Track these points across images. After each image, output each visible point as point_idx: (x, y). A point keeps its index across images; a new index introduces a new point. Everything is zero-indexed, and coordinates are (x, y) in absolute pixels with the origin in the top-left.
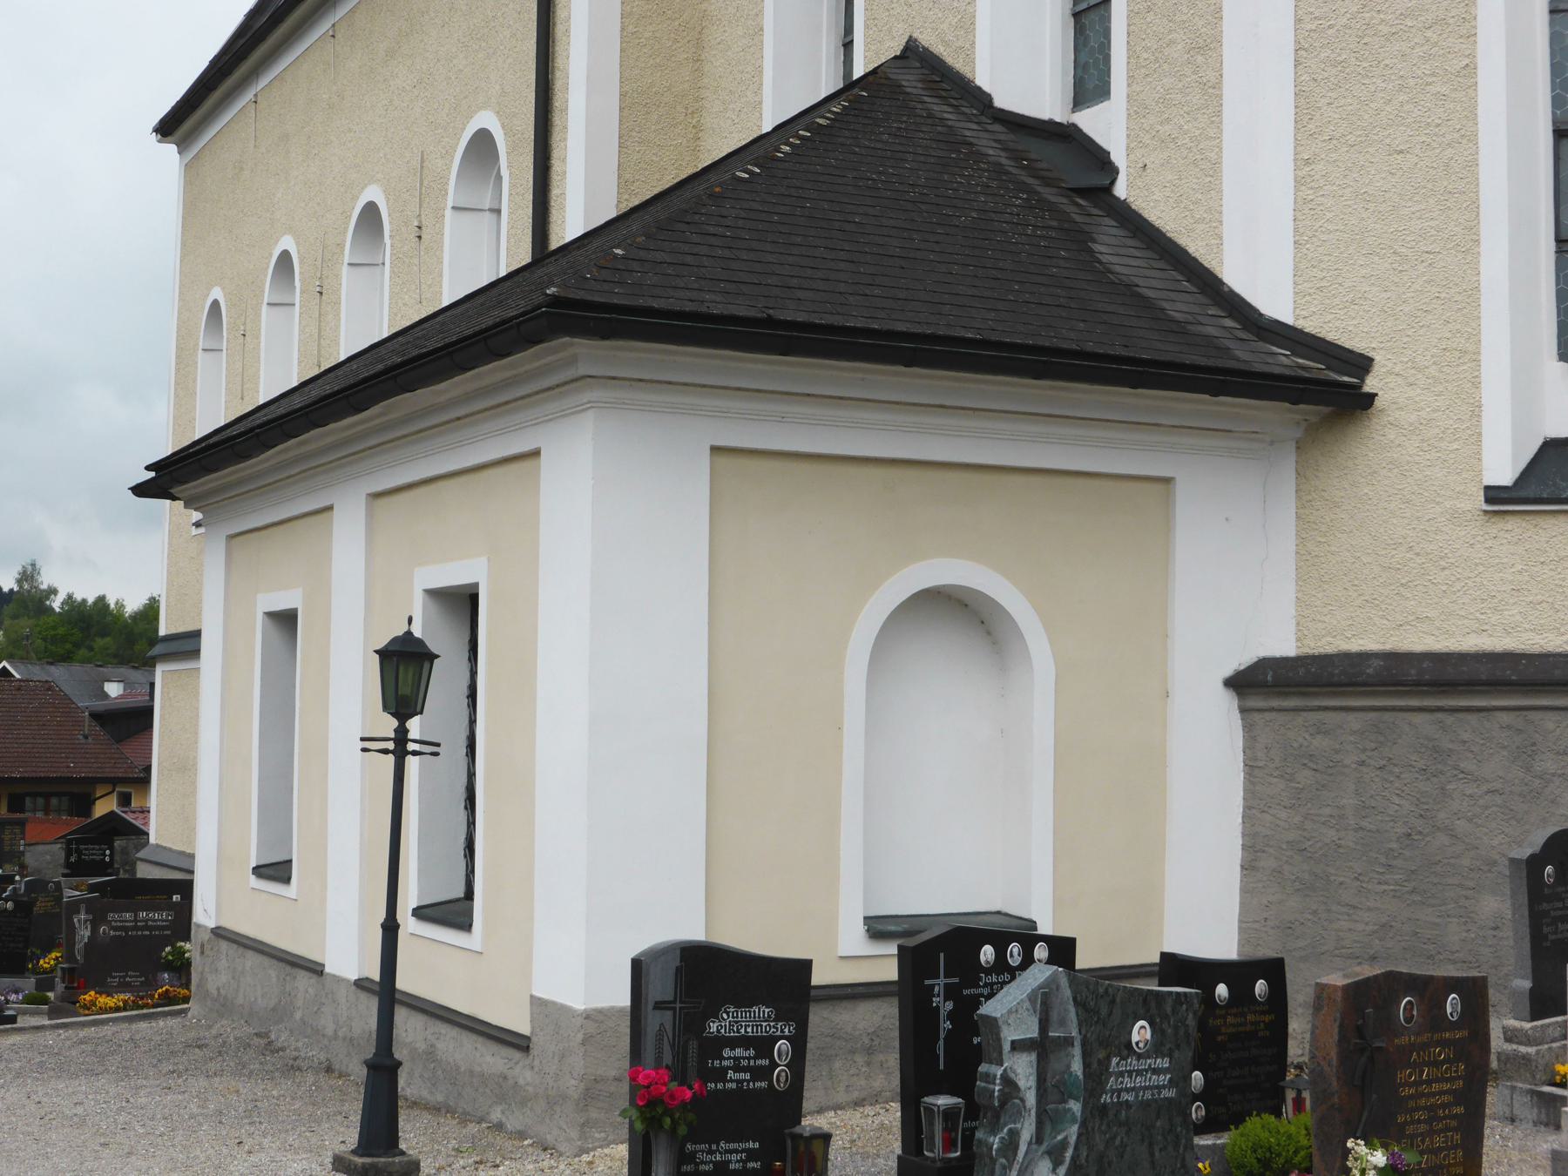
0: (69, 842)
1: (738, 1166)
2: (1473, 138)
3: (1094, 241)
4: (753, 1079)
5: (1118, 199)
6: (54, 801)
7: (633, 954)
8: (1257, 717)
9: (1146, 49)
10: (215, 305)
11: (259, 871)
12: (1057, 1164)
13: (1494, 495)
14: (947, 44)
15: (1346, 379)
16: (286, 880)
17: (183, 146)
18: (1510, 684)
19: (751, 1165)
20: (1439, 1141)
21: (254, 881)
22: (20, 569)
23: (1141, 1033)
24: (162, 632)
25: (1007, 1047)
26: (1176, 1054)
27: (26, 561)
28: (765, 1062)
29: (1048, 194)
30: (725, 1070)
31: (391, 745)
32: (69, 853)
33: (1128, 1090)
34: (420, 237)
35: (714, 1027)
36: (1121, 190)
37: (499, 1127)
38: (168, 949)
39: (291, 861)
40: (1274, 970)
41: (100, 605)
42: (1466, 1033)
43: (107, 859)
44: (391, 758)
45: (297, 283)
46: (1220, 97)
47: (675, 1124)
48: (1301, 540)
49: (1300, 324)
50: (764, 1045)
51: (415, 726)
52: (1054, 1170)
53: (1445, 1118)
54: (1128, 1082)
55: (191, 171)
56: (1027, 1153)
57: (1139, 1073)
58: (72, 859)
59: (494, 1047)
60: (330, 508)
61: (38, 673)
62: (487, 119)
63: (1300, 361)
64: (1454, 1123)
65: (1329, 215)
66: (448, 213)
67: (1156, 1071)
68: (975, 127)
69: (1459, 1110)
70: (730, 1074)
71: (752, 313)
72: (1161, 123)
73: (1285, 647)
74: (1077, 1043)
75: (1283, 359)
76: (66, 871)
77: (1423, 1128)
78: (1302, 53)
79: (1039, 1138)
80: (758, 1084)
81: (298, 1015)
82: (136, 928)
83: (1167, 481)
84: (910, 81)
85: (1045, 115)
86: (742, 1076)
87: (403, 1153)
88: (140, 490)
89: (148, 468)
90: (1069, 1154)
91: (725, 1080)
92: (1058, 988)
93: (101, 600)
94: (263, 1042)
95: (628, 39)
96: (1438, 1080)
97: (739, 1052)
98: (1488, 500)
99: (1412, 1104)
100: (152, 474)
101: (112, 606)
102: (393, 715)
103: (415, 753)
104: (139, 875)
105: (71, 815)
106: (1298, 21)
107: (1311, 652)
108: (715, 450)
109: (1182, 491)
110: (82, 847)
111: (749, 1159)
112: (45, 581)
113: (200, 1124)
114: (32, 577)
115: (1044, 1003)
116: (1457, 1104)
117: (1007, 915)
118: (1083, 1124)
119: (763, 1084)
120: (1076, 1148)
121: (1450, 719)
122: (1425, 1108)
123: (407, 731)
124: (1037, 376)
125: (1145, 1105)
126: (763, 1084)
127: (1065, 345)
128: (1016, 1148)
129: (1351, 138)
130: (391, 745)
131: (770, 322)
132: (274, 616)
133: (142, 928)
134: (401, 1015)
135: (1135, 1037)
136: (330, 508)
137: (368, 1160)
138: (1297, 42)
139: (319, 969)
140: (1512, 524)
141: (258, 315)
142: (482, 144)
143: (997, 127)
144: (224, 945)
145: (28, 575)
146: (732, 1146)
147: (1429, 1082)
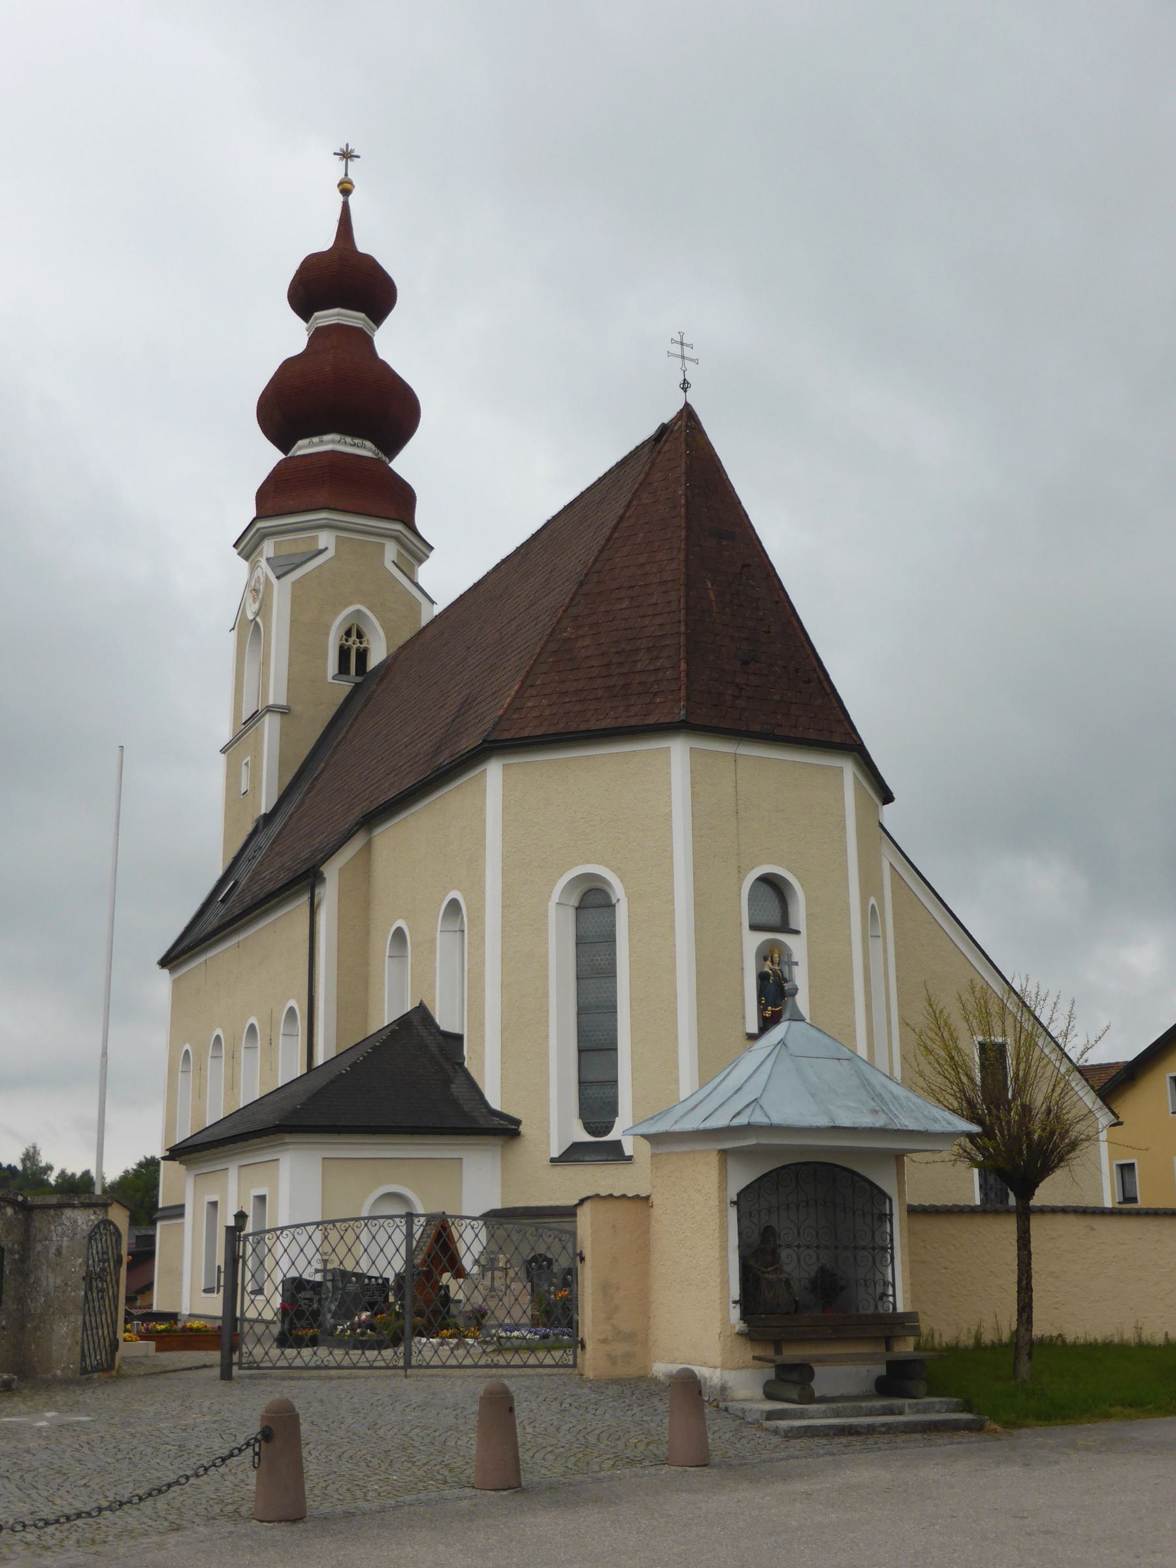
2: (548, 1056)
3: (452, 1083)
10: (187, 1052)
13: (553, 1160)
21: (204, 1295)
22: (24, 1150)
24: (160, 1206)
27: (29, 1144)
41: (86, 1177)
55: (175, 983)
60: (228, 1169)
62: (292, 1003)
73: (497, 1205)
83: (461, 1159)
108: (323, 1158)
109: (464, 1161)
114: (34, 1157)
131: (336, 1126)
136: (228, 1169)
140: (558, 1169)
145: (30, 1157)
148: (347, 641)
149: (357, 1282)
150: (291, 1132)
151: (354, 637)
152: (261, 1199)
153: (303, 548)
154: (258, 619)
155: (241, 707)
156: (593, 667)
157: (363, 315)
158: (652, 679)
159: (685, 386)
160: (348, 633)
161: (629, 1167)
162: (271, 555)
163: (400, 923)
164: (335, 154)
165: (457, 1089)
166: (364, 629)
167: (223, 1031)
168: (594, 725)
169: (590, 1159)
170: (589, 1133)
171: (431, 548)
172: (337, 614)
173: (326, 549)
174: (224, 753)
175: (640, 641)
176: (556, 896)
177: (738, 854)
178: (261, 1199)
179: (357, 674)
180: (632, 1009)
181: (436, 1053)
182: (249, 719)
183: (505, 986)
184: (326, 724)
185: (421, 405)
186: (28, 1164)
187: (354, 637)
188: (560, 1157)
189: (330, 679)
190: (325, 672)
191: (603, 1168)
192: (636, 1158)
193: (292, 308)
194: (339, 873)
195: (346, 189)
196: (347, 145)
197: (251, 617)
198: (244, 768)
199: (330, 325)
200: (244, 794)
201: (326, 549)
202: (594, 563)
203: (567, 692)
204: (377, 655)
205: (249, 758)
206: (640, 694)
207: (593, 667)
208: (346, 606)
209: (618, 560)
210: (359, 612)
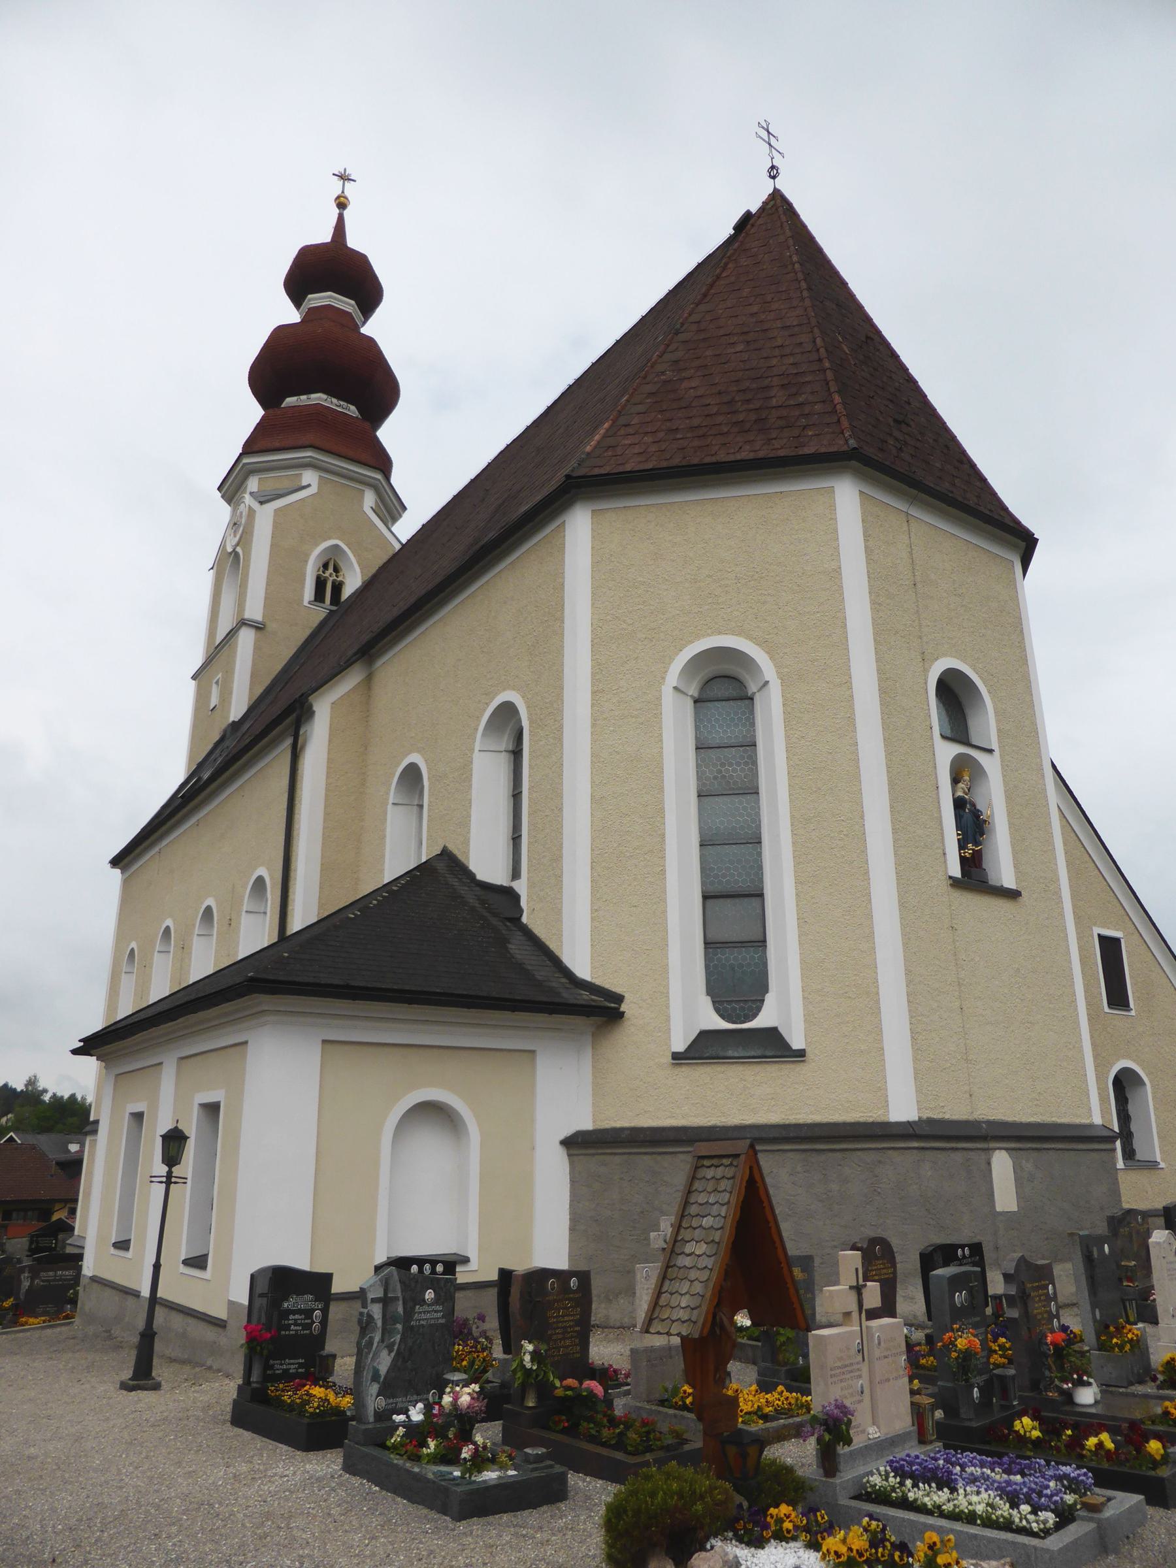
0: (32, 1236)
1: (294, 1371)
3: (509, 943)
4: (303, 1330)
5: (523, 923)
6: (30, 1213)
7: (253, 1270)
8: (575, 1158)
9: (535, 858)
10: (132, 950)
11: (186, 1262)
12: (390, 1351)
13: (676, 1056)
14: (459, 850)
15: (613, 1005)
16: (127, 1249)
17: (123, 870)
18: (683, 1141)
19: (300, 1370)
20: (568, 1342)
21: (113, 1251)
22: (27, 1078)
23: (429, 1295)
25: (369, 1301)
26: (446, 1304)
27: (31, 1074)
28: (309, 1321)
29: (494, 921)
30: (290, 1325)
31: (164, 1179)
32: (31, 1243)
33: (423, 1320)
34: (230, 924)
35: (286, 1305)
36: (524, 919)
37: (210, 1368)
38: (71, 1291)
39: (130, 1240)
40: (584, 1278)
42: (580, 1295)
43: (53, 1245)
44: (164, 1185)
45: (172, 942)
46: (562, 881)
47: (262, 1349)
48: (594, 1076)
49: (593, 981)
50: (308, 1313)
51: (176, 1171)
52: (389, 1355)
53: (571, 1332)
54: (423, 1316)
55: (126, 883)
56: (377, 1346)
57: (428, 1312)
58: (33, 1247)
59: (212, 1328)
60: (161, 1064)
61: (32, 1139)
62: (262, 871)
63: (593, 997)
64: (575, 1334)
65: (605, 934)
66: (244, 913)
67: (436, 1312)
68: (466, 888)
69: (577, 1329)
70: (292, 1327)
71: (342, 983)
72: (540, 891)
73: (587, 1125)
74: (401, 1299)
75: (585, 996)
76: (29, 1254)
77: (560, 1336)
78: (594, 864)
79: (382, 1340)
80: (305, 1332)
81: (127, 1319)
82: (54, 1280)
83: (533, 1052)
84: (441, 866)
85: (499, 883)
86: (298, 1328)
87: (153, 1379)
88: (75, 1052)
89: (80, 1041)
90: (396, 1348)
91: (290, 1330)
92: (393, 1275)
93: (73, 1097)
94: (106, 1334)
95: (326, 838)
96: (567, 1316)
97: (297, 1317)
98: (673, 1058)
99: (555, 1325)
100: (82, 1044)
101: (79, 1099)
102: (167, 1165)
103: (175, 1183)
104: (67, 1251)
105: (38, 1221)
106: (592, 850)
107: (599, 1128)
108: (324, 1042)
109: (538, 1053)
110: (40, 1239)
111: (299, 1368)
112: (41, 1085)
113: (62, 1374)
115: (386, 1282)
116: (577, 1325)
117: (458, 1255)
118: (403, 1334)
119: (308, 1332)
120: (399, 1345)
121: (659, 1158)
122: (561, 1328)
123: (172, 1172)
124: (469, 1008)
125: (431, 1325)
126: (308, 1332)
127: (481, 994)
128: (372, 1344)
129: (614, 901)
130: (164, 1179)
131: (348, 987)
132: (133, 1114)
133: (58, 1280)
134: (158, 1308)
135: (427, 1297)
137: (135, 1382)
138: (592, 859)
139: (137, 1293)
140: (684, 1069)
141: (154, 954)
142: (260, 881)
143: (478, 888)
144: (95, 1285)
146: (292, 1361)
147: (563, 1316)
148: (324, 572)
149: (436, 1301)
150: (273, 992)
151: (331, 570)
152: (212, 1109)
153: (286, 484)
154: (239, 549)
155: (216, 628)
156: (709, 405)
157: (353, 302)
158: (797, 413)
159: (773, 171)
160: (325, 566)
161: (799, 1068)
162: (255, 489)
163: (415, 758)
164: (334, 174)
165: (517, 948)
166: (341, 564)
167: (174, 920)
168: (722, 457)
169: (736, 1054)
170: (723, 1017)
171: (405, 508)
172: (317, 545)
173: (309, 485)
174: (194, 680)
175: (770, 379)
176: (673, 676)
177: (920, 637)
178: (212, 1109)
179: (331, 604)
180: (794, 834)
181: (477, 905)
182: (223, 640)
183: (596, 801)
184: (300, 643)
185: (400, 401)
186: (30, 1088)
187: (331, 570)
188: (686, 1050)
189: (306, 603)
190: (302, 596)
191: (757, 1068)
192: (809, 1054)
193: (288, 295)
194: (332, 708)
195: (342, 204)
196: (345, 170)
197: (229, 549)
198: (214, 686)
199: (322, 306)
200: (212, 710)
201: (309, 485)
202: (690, 315)
203: (677, 429)
204: (352, 583)
205: (220, 676)
206: (783, 428)
207: (709, 405)
208: (325, 540)
209: (721, 311)
210: (337, 546)
